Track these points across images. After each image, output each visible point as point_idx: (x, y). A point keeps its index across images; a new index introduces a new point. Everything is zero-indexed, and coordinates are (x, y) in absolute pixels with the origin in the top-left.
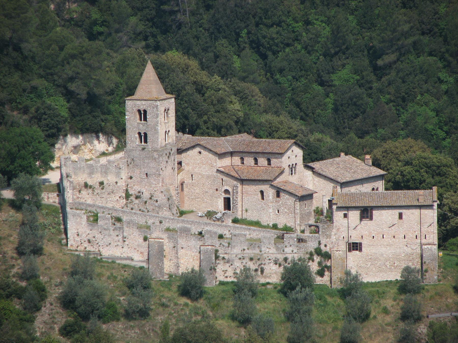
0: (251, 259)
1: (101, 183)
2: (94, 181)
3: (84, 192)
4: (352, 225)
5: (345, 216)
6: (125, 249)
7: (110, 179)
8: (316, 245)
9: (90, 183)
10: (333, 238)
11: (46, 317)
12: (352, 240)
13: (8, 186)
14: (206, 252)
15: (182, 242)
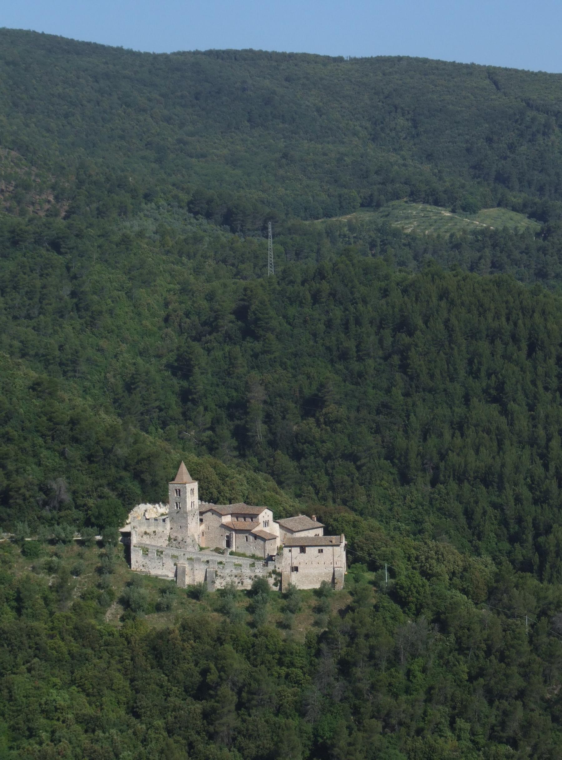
0: (236, 576)
1: (154, 532)
2: (150, 530)
3: (145, 537)
4: (294, 556)
5: (290, 551)
6: (164, 570)
7: (160, 529)
8: (273, 568)
9: (148, 532)
10: (283, 564)
11: (113, 611)
12: (294, 565)
13: (99, 534)
14: (210, 572)
15: (196, 566)
